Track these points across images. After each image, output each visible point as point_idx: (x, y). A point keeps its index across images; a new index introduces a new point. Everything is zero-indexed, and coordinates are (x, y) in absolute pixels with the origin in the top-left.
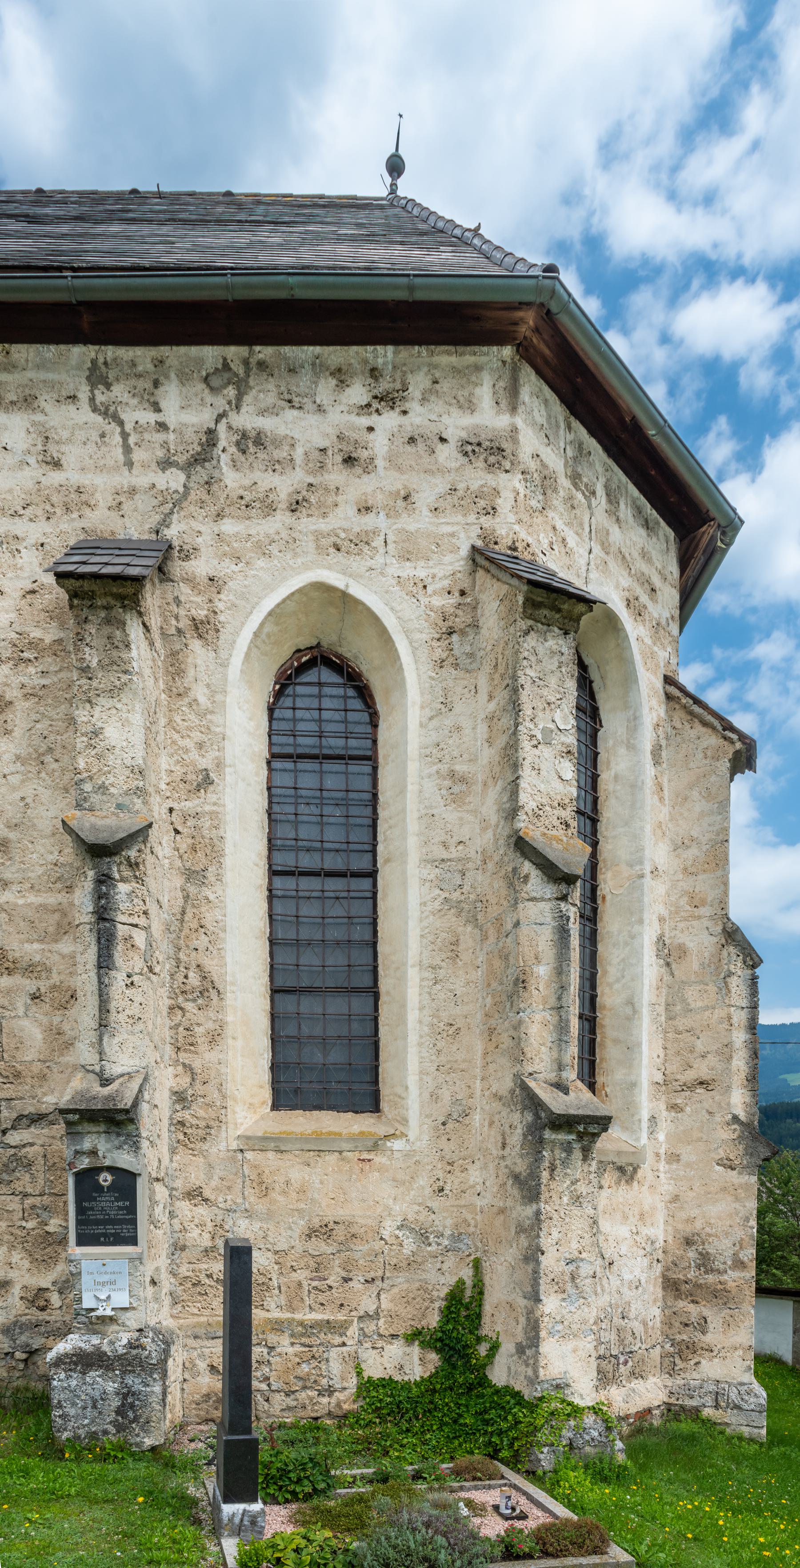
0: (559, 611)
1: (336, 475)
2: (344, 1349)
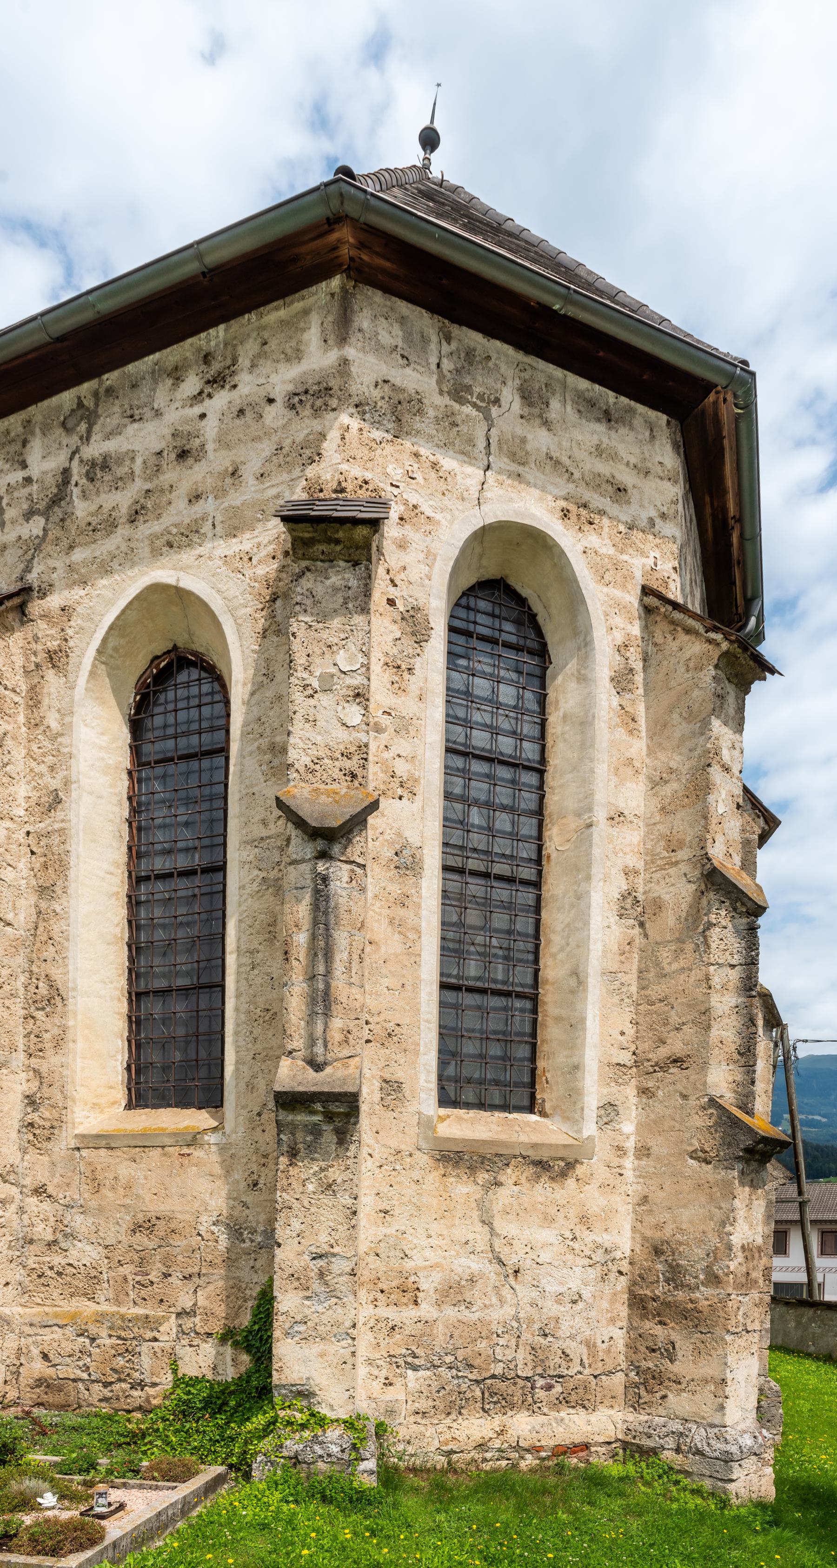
0: (337, 542)
2: (155, 1344)
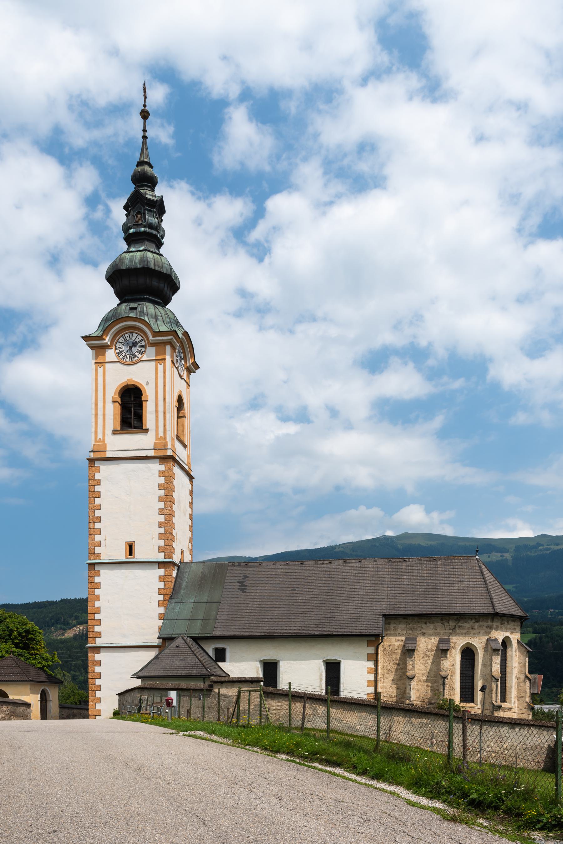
1: (471, 630)
